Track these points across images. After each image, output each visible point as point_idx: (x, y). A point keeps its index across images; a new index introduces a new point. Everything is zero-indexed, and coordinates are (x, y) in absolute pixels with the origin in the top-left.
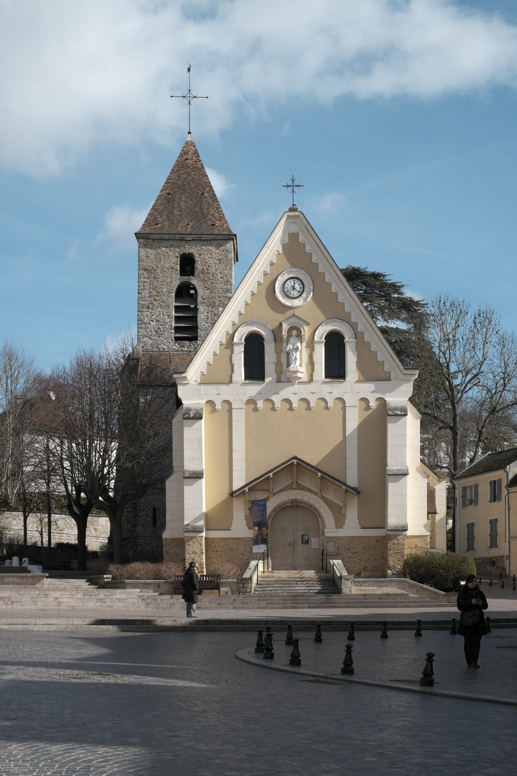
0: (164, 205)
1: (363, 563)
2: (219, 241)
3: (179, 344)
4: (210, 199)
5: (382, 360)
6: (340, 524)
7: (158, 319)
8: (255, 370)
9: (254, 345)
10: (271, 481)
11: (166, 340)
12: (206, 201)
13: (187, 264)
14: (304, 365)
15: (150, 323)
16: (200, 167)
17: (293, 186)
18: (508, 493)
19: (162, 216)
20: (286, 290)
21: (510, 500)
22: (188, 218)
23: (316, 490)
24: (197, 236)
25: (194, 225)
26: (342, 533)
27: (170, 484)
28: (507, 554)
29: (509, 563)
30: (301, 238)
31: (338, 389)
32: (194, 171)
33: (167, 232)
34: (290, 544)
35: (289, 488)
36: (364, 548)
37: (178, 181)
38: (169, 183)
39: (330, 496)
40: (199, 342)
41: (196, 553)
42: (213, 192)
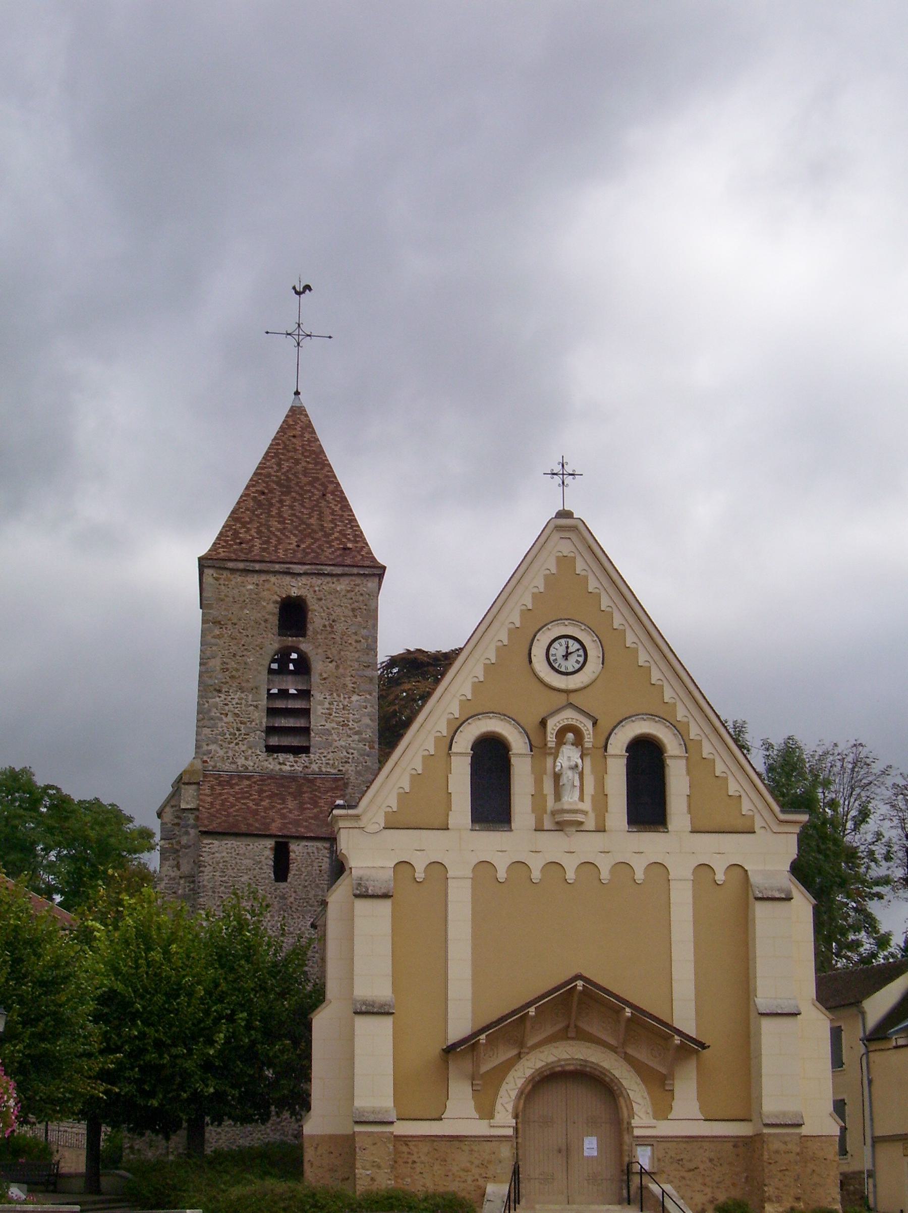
0: (253, 512)
1: (708, 1190)
2: (353, 578)
3: (274, 759)
4: (336, 505)
5: (737, 794)
6: (662, 1111)
7: (236, 711)
8: (492, 804)
9: (491, 758)
10: (528, 1024)
11: (250, 751)
12: (330, 508)
13: (293, 615)
14: (588, 798)
15: (221, 719)
16: (318, 451)
17: (563, 474)
18: (868, 1052)
19: (249, 530)
20: (552, 658)
21: (871, 1065)
22: (295, 535)
23: (613, 1042)
24: (313, 567)
25: (308, 547)
26: (665, 1128)
27: (323, 1023)
28: (868, 1166)
29: (875, 1186)
30: (580, 566)
31: (648, 846)
32: (306, 457)
33: (258, 558)
34: (560, 1151)
35: (563, 1035)
36: (711, 1160)
37: (277, 471)
38: (261, 474)
39: (642, 1055)
40: (312, 756)
41: (379, 1167)
42: (342, 492)
